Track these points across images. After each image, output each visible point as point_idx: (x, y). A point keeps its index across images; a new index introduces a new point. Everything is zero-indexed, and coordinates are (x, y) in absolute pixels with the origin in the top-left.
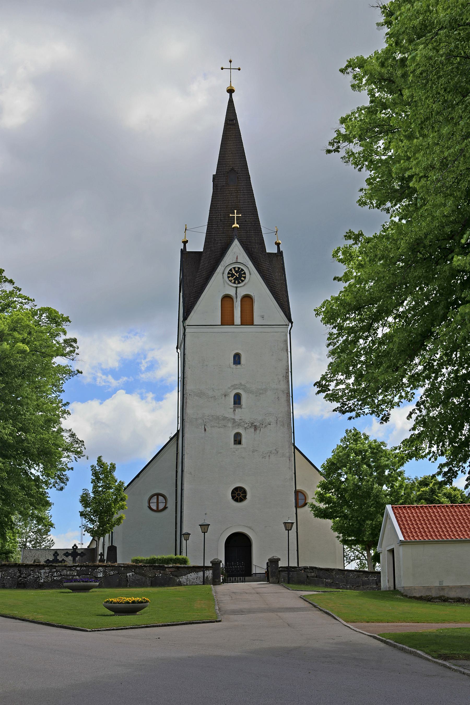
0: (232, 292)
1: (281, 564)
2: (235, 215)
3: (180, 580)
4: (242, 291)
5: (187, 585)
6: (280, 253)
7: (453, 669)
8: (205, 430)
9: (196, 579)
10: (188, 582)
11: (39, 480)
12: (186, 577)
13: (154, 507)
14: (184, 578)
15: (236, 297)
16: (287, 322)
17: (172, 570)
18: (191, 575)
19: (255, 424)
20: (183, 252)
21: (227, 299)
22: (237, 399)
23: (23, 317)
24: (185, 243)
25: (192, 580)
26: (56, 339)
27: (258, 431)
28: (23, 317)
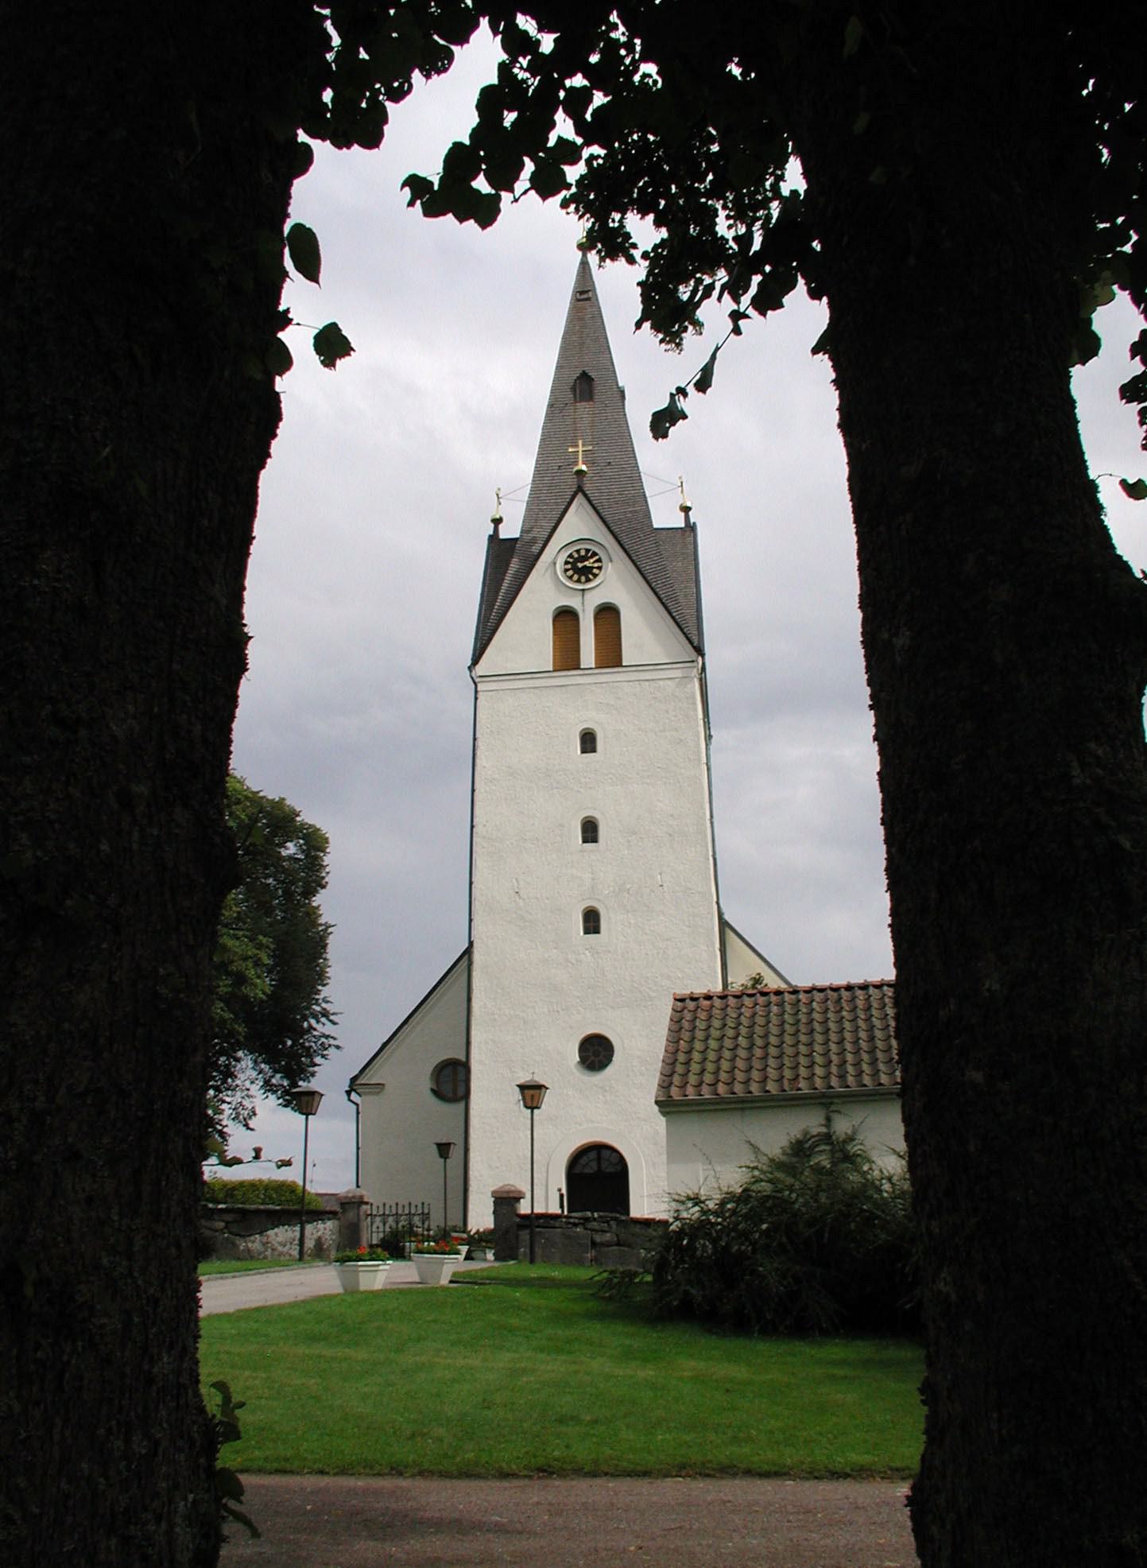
0: (574, 602)
1: (524, 1208)
2: (581, 449)
3: (250, 1245)
4: (595, 599)
6: (690, 528)
7: (370, 1468)
9: (291, 1244)
11: (702, 1221)
13: (447, 1089)
15: (584, 610)
16: (693, 655)
17: (229, 1217)
20: (494, 538)
21: (565, 618)
22: (590, 831)
24: (497, 522)
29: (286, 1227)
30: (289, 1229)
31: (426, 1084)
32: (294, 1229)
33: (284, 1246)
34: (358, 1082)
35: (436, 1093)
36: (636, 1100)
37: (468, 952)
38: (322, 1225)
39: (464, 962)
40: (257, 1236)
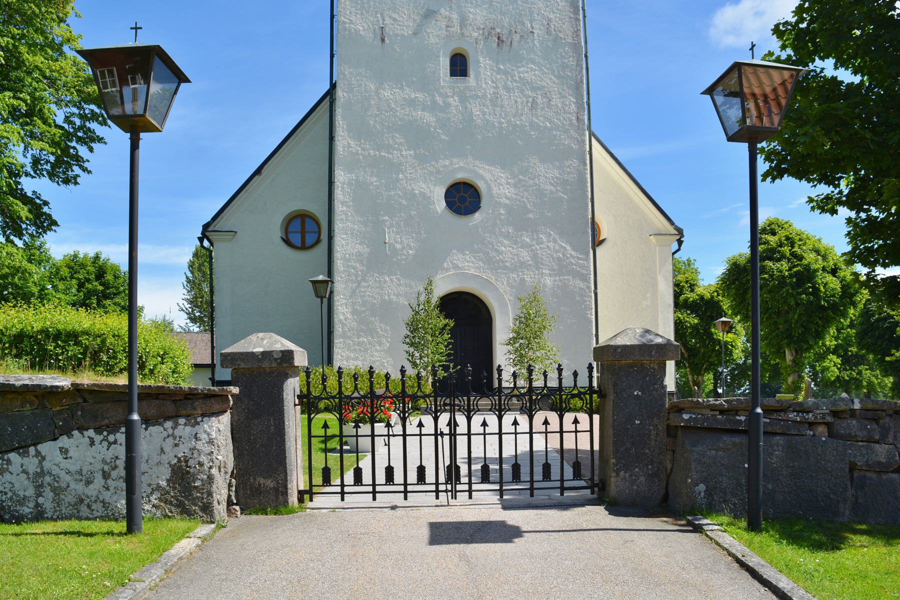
5: (39, 516)
8: (383, 40)
9: (106, 476)
10: (47, 501)
12: (31, 464)
13: (296, 239)
14: (15, 467)
18: (64, 451)
19: (498, 30)
23: (53, 124)
25: (78, 488)
26: (760, 125)
27: (505, 47)
28: (53, 124)
29: (91, 433)
30: (98, 438)
31: (277, 233)
32: (111, 438)
33: (88, 483)
34: (211, 229)
35: (287, 241)
36: (503, 248)
37: (331, 94)
38: (188, 429)
39: (325, 104)
40: (13, 456)
